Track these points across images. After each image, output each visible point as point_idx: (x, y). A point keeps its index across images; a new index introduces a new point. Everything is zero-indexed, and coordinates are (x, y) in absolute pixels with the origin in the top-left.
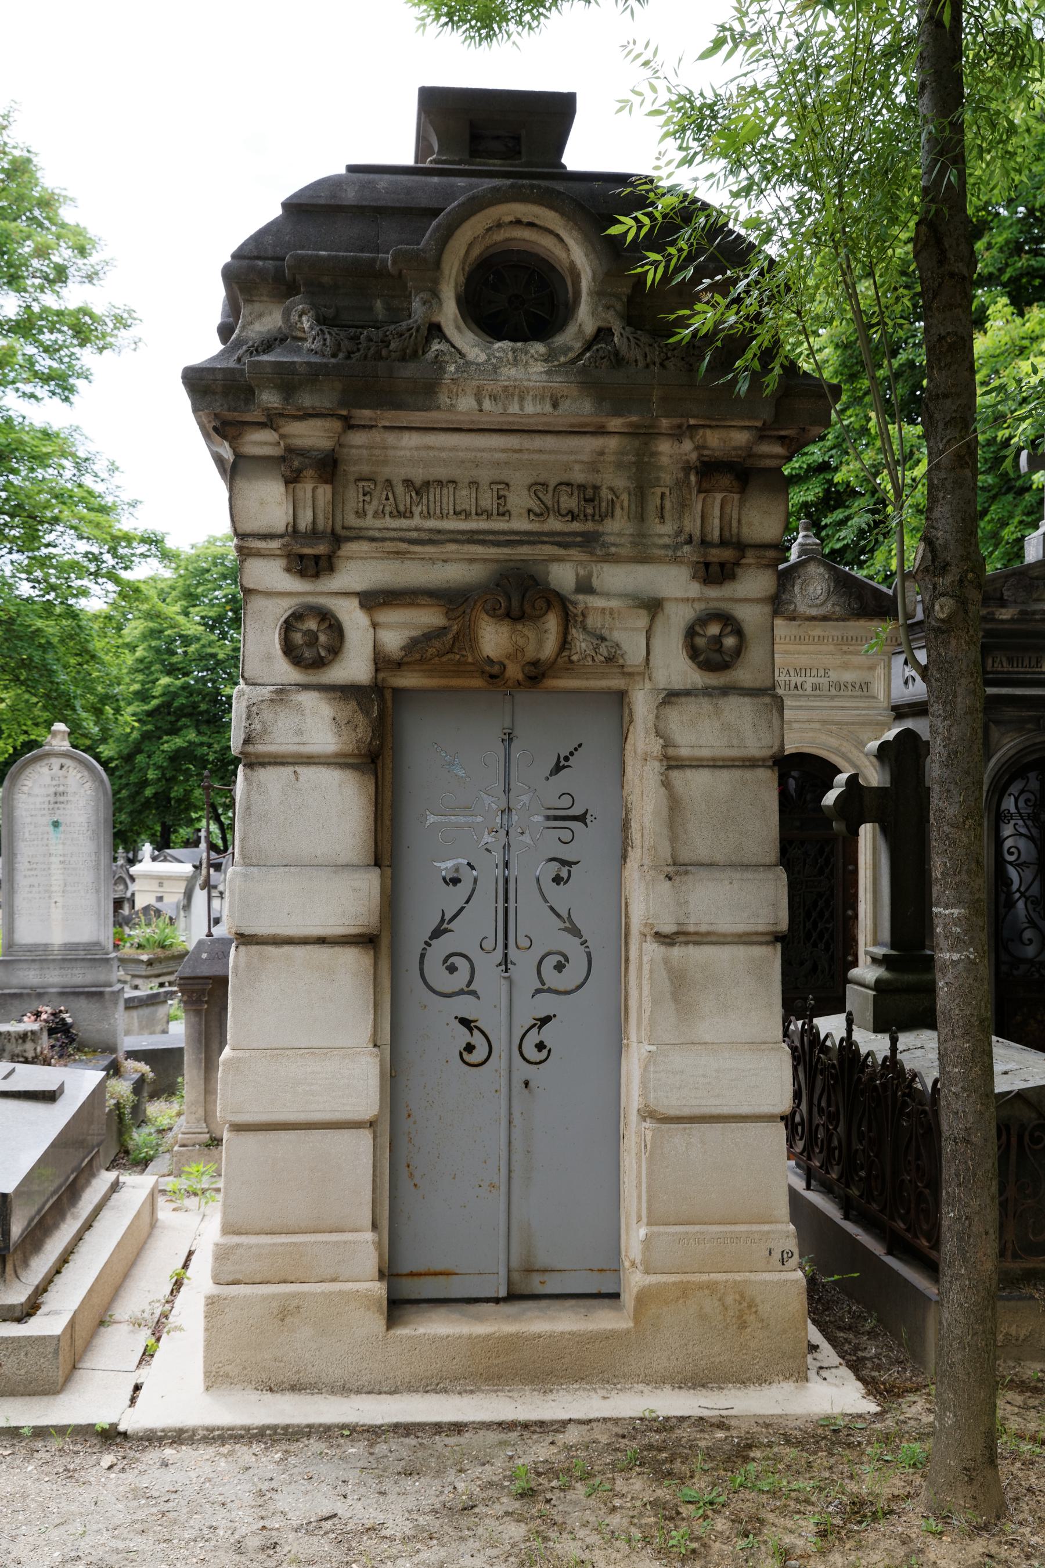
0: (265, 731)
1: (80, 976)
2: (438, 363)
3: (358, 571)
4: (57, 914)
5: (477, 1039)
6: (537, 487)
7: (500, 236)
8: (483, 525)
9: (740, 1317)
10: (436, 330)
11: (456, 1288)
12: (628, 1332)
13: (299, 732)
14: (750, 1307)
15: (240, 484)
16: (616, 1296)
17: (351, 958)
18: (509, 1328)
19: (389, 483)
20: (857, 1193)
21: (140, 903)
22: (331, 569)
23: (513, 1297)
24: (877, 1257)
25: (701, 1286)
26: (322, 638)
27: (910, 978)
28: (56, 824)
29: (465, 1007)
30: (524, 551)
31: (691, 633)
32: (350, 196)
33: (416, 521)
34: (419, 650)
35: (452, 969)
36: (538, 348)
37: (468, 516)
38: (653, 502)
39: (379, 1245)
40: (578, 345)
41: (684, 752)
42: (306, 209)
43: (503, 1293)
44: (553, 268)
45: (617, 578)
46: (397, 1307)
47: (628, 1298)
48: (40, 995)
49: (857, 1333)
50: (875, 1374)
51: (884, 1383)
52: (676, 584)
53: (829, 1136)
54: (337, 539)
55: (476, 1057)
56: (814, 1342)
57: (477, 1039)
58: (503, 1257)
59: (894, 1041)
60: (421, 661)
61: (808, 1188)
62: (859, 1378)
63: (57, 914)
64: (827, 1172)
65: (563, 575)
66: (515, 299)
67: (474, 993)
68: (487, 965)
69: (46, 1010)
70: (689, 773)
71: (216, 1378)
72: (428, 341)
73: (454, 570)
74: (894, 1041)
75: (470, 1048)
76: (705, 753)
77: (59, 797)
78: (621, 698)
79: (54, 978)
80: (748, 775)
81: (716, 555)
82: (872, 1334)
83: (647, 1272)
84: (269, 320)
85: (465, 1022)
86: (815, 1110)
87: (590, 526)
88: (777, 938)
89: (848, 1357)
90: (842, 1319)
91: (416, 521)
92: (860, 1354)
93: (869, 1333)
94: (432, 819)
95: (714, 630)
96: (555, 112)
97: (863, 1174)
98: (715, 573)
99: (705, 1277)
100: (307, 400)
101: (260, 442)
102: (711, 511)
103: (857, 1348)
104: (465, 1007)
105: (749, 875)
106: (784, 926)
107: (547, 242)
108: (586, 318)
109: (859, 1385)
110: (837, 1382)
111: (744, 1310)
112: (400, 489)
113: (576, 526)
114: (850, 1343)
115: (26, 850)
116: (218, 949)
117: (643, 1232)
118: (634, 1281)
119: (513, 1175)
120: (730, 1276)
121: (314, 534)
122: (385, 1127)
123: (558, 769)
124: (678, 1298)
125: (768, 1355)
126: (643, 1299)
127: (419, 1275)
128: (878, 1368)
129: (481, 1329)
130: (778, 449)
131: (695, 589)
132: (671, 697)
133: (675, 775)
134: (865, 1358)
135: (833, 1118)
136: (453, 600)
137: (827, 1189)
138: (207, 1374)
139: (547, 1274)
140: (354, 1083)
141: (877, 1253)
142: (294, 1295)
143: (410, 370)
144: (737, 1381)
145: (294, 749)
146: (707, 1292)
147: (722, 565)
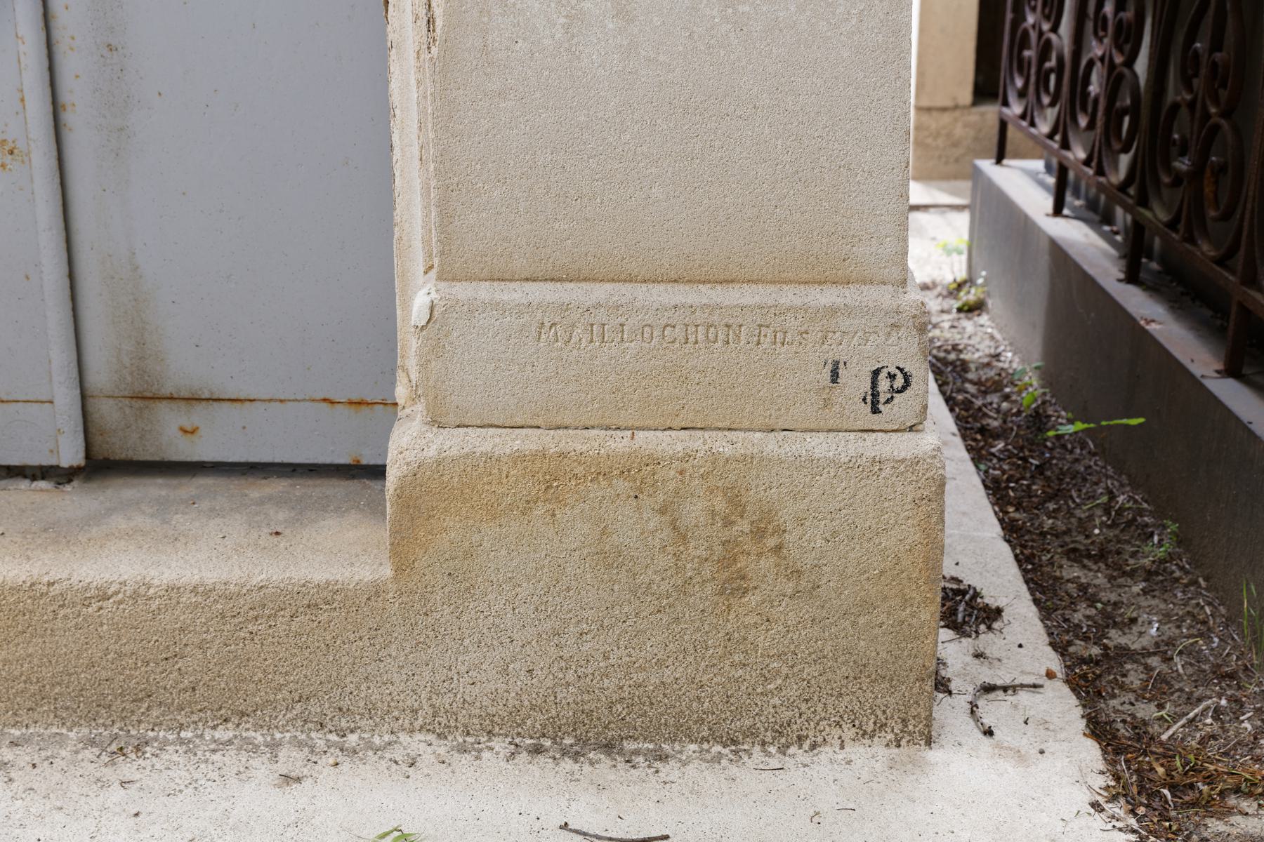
9: (727, 561)
12: (377, 591)
14: (758, 533)
16: (378, 472)
20: (1082, 155)
23: (99, 466)
24: (1196, 384)
25: (602, 471)
43: (71, 454)
49: (1120, 572)
50: (1146, 711)
51: (1167, 755)
53: (1115, 81)
56: (991, 597)
58: (60, 357)
61: (1058, 211)
62: (1098, 729)
64: (1033, 124)
82: (1157, 579)
83: (437, 422)
86: (1090, 26)
89: (1078, 647)
90: (1084, 527)
92: (1116, 638)
93: (1149, 575)
97: (1182, 165)
99: (619, 443)
103: (1110, 619)
109: (1091, 752)
110: (1025, 741)
111: (741, 541)
114: (1092, 601)
119: (68, 117)
120: (697, 442)
124: (531, 502)
125: (814, 670)
128: (1159, 688)
134: (1125, 653)
135: (1127, 38)
137: (1098, 215)
139: (200, 407)
141: (1197, 370)
144: (714, 737)
146: (621, 485)
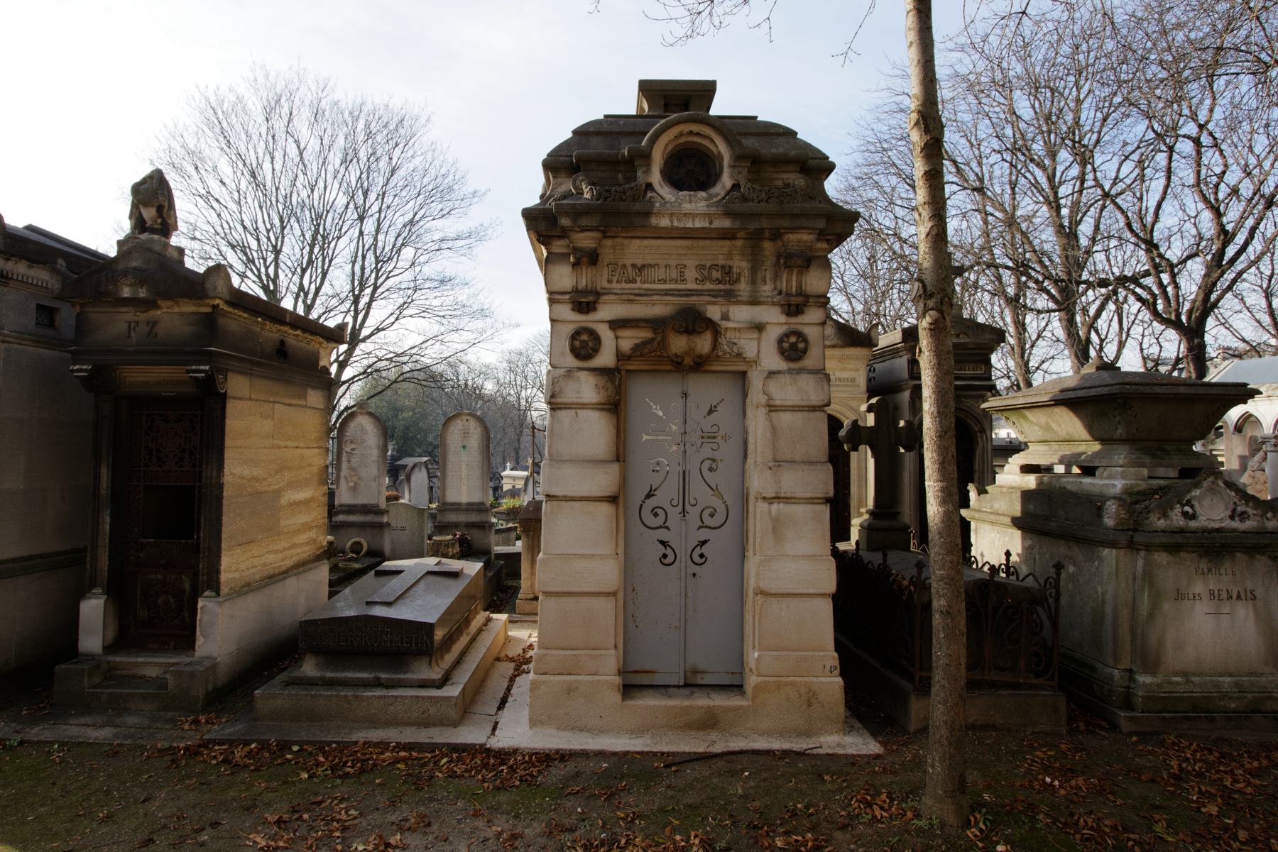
0: (561, 391)
1: (474, 518)
2: (651, 201)
3: (608, 311)
4: (464, 488)
5: (669, 551)
6: (700, 267)
7: (682, 140)
8: (673, 286)
10: (649, 186)
11: (658, 680)
13: (578, 392)
15: (551, 267)
17: (606, 509)
18: (687, 703)
19: (624, 266)
21: (506, 488)
22: (595, 309)
25: (787, 684)
26: (591, 344)
27: (885, 523)
28: (464, 447)
29: (663, 535)
30: (694, 299)
31: (780, 341)
32: (606, 127)
33: (638, 285)
34: (639, 350)
35: (656, 515)
36: (703, 194)
37: (665, 282)
38: (759, 275)
39: (617, 657)
40: (723, 193)
41: (778, 403)
42: (583, 133)
44: (708, 156)
45: (741, 314)
46: (628, 690)
47: (749, 688)
48: (456, 525)
52: (773, 317)
54: (598, 294)
55: (667, 561)
57: (669, 551)
59: (885, 555)
60: (641, 356)
63: (464, 488)
65: (714, 312)
66: (691, 169)
67: (667, 528)
68: (674, 514)
69: (458, 534)
70: (781, 414)
71: (534, 722)
72: (645, 191)
73: (658, 309)
74: (885, 555)
75: (665, 556)
76: (789, 403)
77: (465, 434)
78: (743, 375)
79: (463, 518)
80: (812, 415)
81: (794, 300)
83: (759, 675)
84: (567, 185)
85: (663, 543)
87: (728, 287)
88: (828, 500)
91: (638, 285)
94: (645, 437)
95: (793, 339)
96: (706, 90)
98: (793, 309)
100: (584, 222)
101: (559, 246)
102: (789, 282)
104: (663, 535)
105: (812, 467)
106: (831, 494)
107: (706, 143)
108: (726, 180)
111: (811, 698)
112: (630, 269)
113: (721, 287)
115: (452, 459)
116: (536, 506)
117: (756, 655)
118: (752, 681)
121: (586, 292)
122: (621, 596)
123: (710, 412)
126: (757, 688)
127: (638, 672)
129: (671, 703)
130: (825, 246)
131: (783, 318)
132: (771, 374)
133: (773, 414)
136: (655, 324)
138: (531, 720)
140: (607, 573)
142: (576, 681)
143: (637, 207)
145: (575, 400)
147: (797, 306)
